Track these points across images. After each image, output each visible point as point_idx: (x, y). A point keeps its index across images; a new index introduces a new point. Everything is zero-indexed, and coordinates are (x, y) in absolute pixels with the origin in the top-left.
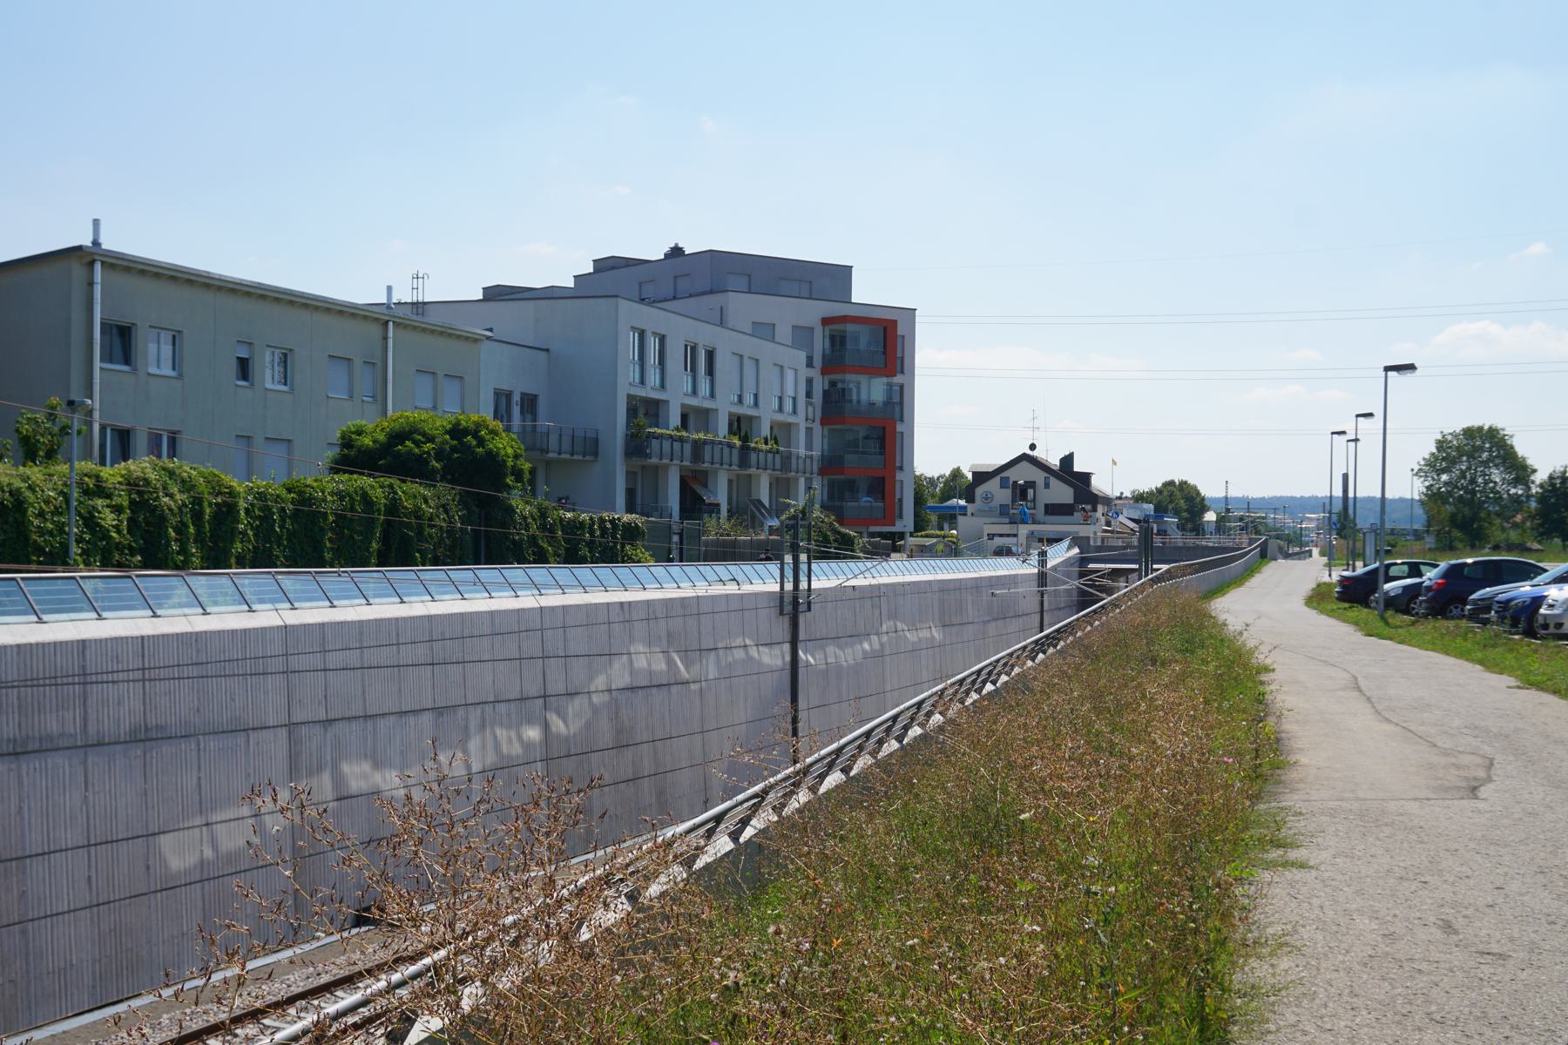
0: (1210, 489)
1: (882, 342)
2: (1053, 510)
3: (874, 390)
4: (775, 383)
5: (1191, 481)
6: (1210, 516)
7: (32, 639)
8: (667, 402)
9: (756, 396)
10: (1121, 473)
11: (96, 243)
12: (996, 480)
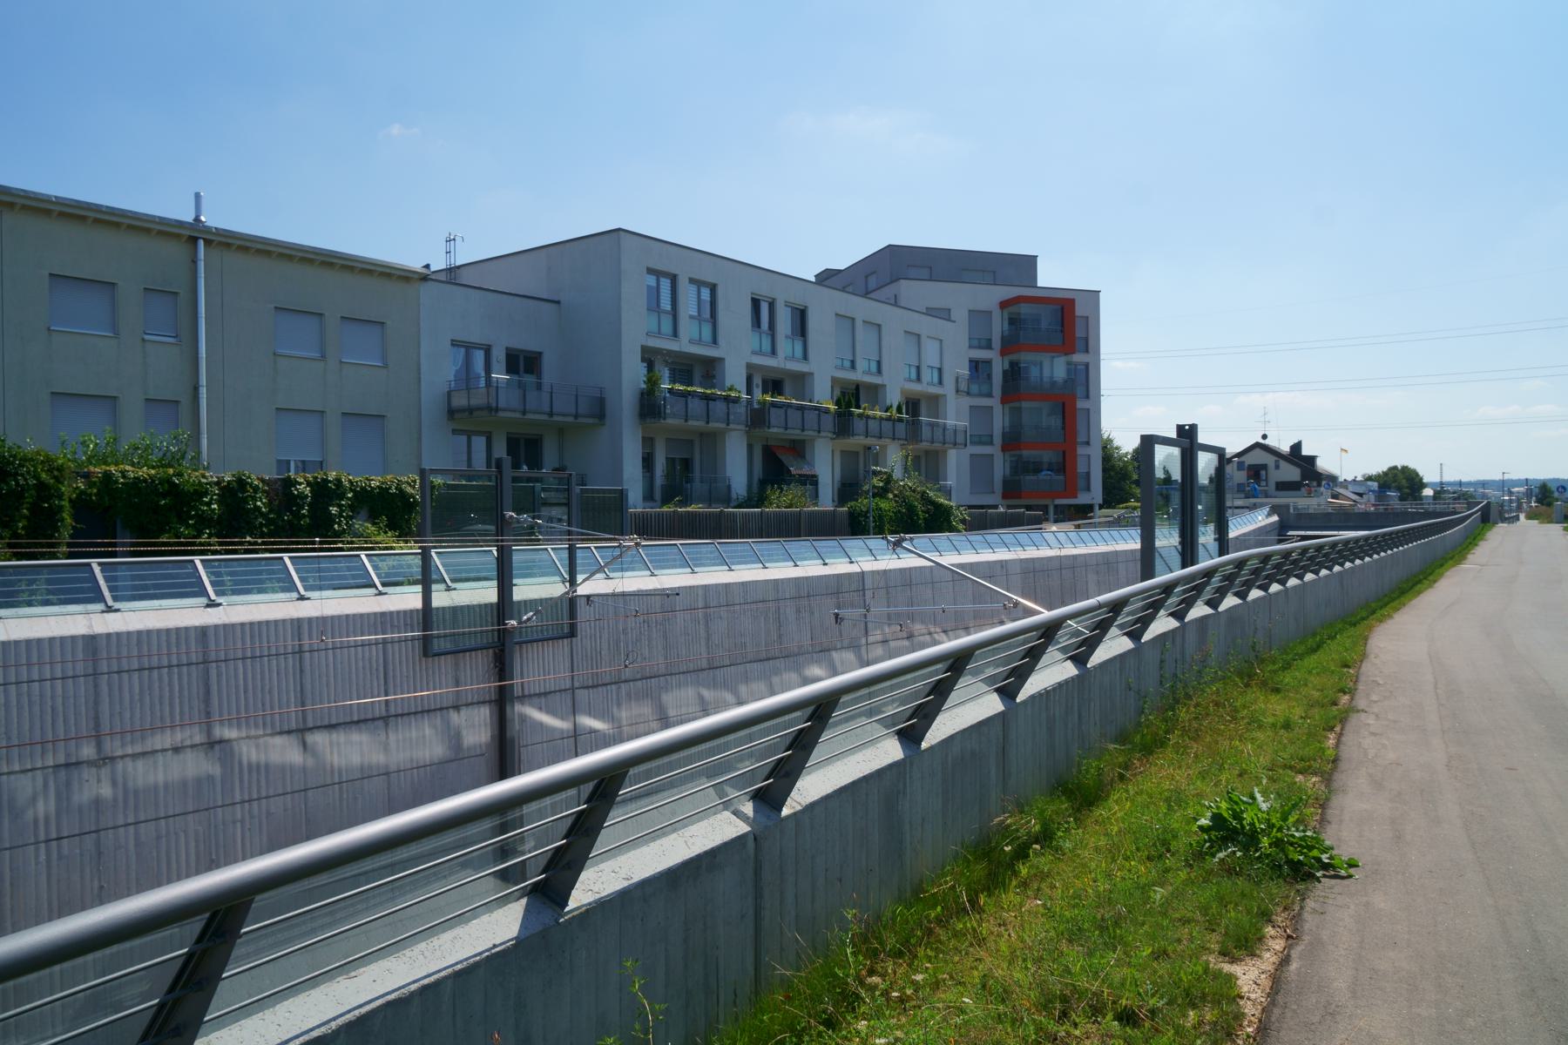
0: (1429, 475)
1: (1065, 323)
2: (1283, 486)
3: (1056, 368)
4: (927, 356)
5: (1412, 466)
6: (1428, 492)
7: (378, 609)
8: (721, 360)
9: (879, 363)
10: (1350, 458)
11: (197, 219)
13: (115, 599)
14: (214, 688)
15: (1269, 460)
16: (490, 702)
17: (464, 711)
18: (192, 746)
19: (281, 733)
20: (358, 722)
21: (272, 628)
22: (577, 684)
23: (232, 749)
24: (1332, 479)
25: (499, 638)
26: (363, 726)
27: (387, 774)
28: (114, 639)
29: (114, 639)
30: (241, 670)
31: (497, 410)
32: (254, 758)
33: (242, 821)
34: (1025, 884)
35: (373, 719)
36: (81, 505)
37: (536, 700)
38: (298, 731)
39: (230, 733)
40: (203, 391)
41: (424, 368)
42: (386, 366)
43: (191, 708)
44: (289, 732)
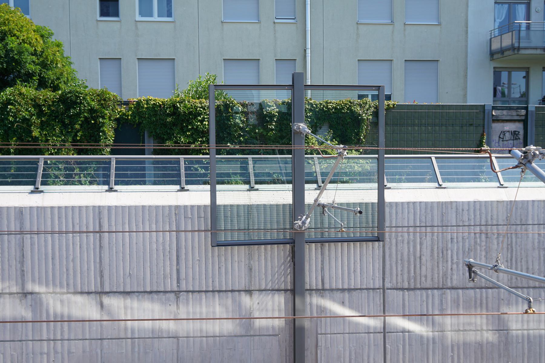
13: (444, 180)
14: (28, 254)
16: (286, 290)
17: (256, 295)
18: (10, 294)
19: (82, 293)
20: (151, 292)
21: (77, 211)
22: (388, 285)
23: (40, 299)
25: (294, 239)
26: (155, 296)
27: (177, 337)
28: (423, 205)
30: (127, 240)
31: (519, 48)
32: (59, 309)
33: (48, 354)
35: (165, 292)
36: (122, 124)
37: (338, 295)
38: (96, 293)
39: (37, 289)
40: (309, 51)
41: (470, 24)
42: (439, 24)
43: (10, 266)
44: (89, 293)
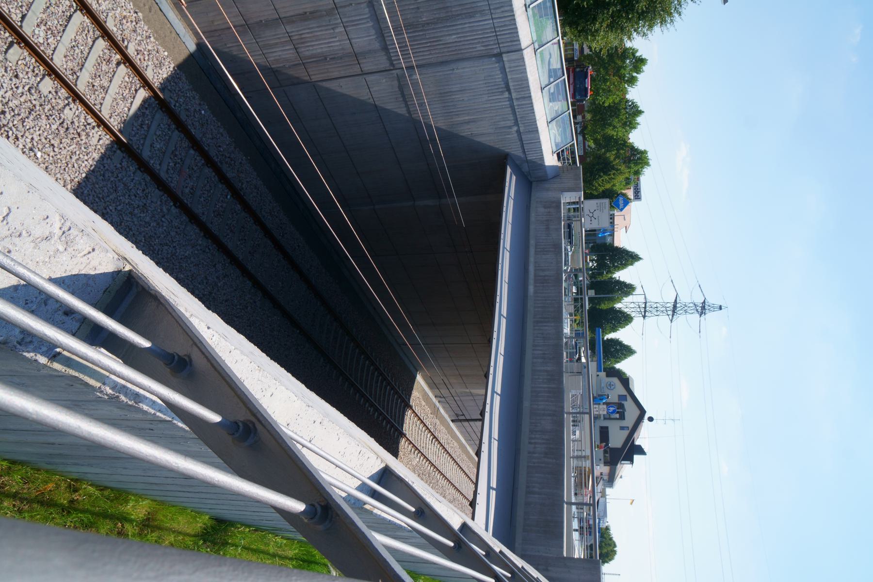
2: (604, 434)
5: (616, 557)
12: (624, 392)
15: (629, 422)
21: (508, 8)
24: (611, 480)
28: (513, 22)
29: (513, 22)
34: (169, 126)
